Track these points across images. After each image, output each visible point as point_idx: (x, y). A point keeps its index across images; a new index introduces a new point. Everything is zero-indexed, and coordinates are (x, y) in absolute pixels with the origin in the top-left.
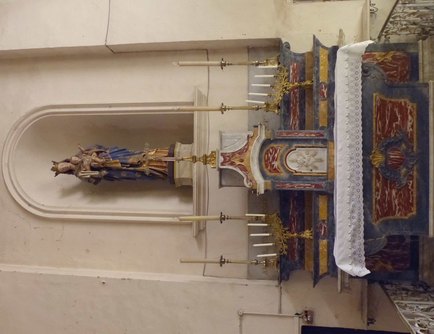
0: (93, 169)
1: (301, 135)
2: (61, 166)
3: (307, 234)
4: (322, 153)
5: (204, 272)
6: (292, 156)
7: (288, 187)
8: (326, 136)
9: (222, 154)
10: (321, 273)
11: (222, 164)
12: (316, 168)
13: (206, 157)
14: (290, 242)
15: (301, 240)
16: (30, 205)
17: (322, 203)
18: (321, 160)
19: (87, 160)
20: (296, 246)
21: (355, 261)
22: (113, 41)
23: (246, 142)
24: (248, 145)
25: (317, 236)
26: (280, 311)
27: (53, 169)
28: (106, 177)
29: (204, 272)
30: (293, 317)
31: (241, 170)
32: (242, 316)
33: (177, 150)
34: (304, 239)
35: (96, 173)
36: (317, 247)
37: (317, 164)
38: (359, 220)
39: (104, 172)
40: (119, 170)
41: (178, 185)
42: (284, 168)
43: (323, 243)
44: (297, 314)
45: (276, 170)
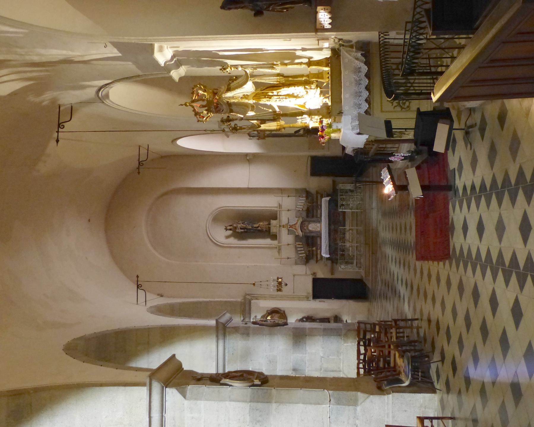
0: (241, 229)
1: (312, 219)
2: (229, 228)
3: (314, 249)
4: (318, 225)
5: (467, 120)
6: (310, 225)
7: (309, 235)
8: (320, 220)
9: (289, 225)
10: (318, 259)
11: (289, 228)
12: (317, 229)
13: (283, 225)
14: (309, 251)
15: (313, 251)
16: (217, 242)
17: (319, 239)
18: (318, 227)
19: (239, 226)
20: (311, 252)
21: (326, 254)
22: (250, 186)
23: (296, 222)
24: (297, 222)
25: (317, 249)
26: (306, 273)
27: (225, 229)
28: (245, 232)
29: (467, 120)
30: (310, 275)
31: (295, 230)
32: (294, 276)
33: (271, 223)
34: (313, 250)
35: (243, 230)
36: (317, 252)
37: (317, 228)
38: (327, 243)
39: (245, 230)
40: (250, 229)
41: (271, 234)
42: (308, 229)
43: (319, 251)
44: (311, 274)
45: (305, 230)
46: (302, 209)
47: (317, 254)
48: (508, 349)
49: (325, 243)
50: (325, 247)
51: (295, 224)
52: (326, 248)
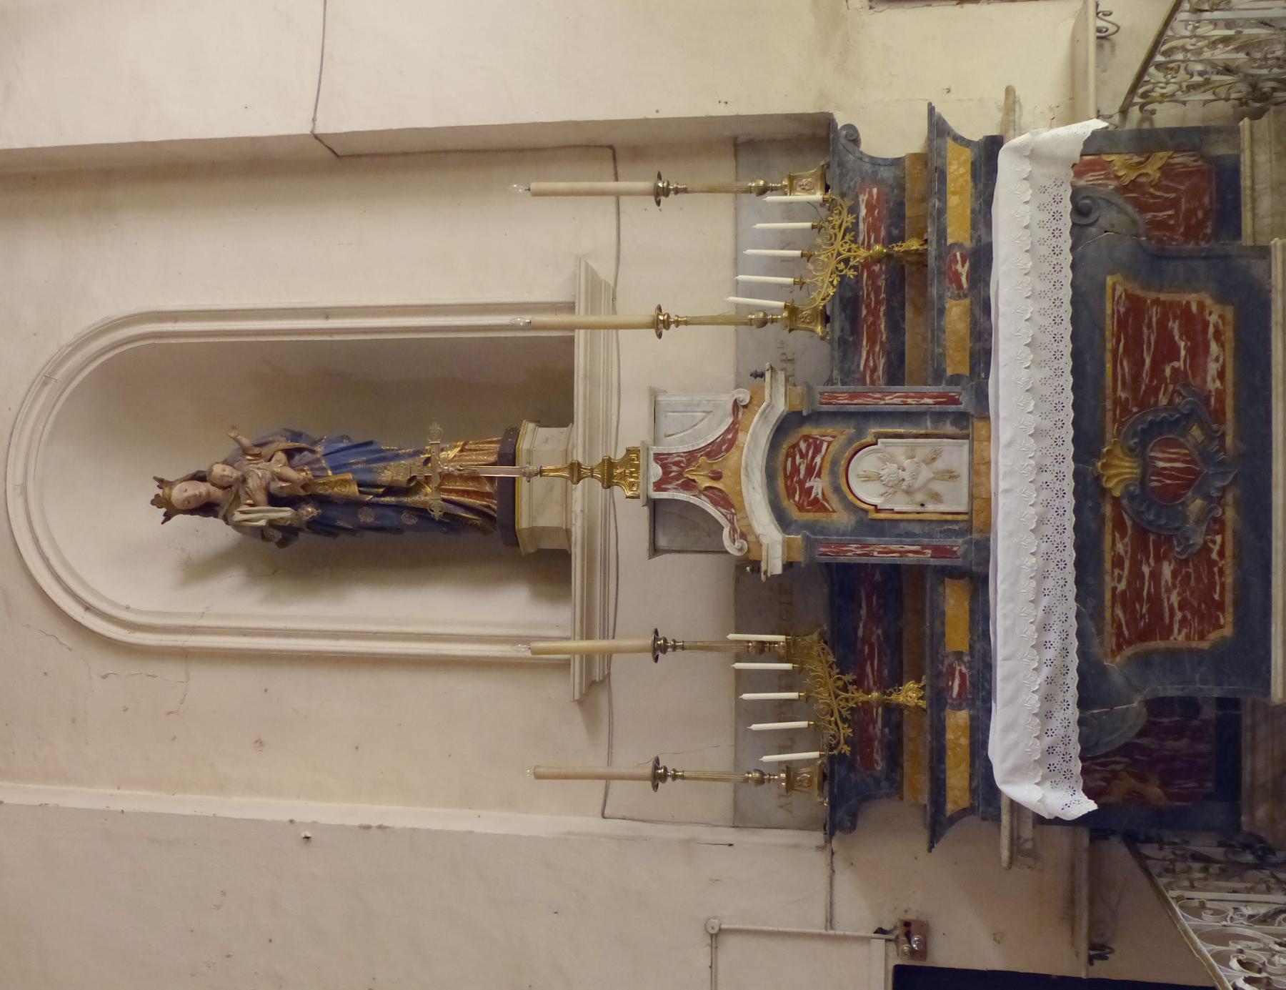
0: (275, 500)
1: (893, 399)
2: (180, 493)
3: (909, 694)
4: (955, 454)
5: (604, 806)
6: (865, 462)
7: (852, 553)
8: (966, 403)
9: (659, 458)
10: (950, 808)
11: (659, 486)
12: (936, 497)
13: (609, 464)
14: (858, 719)
15: (893, 713)
16: (88, 608)
17: (954, 602)
18: (951, 476)
19: (258, 474)
20: (878, 729)
21: (1051, 772)
22: (336, 122)
23: (730, 420)
24: (734, 428)
25: (938, 700)
26: (830, 921)
27: (157, 502)
28: (316, 526)
29: (604, 806)
30: (867, 940)
31: (715, 503)
32: (716, 936)
33: (524, 444)
34: (900, 709)
35: (285, 513)
36: (939, 731)
37: (939, 487)
38: (1065, 652)
39: (309, 511)
40: (352, 504)
41: (528, 547)
42: (843, 498)
43: (958, 719)
44: (880, 931)
45: (817, 505)
48: (1079, 720)
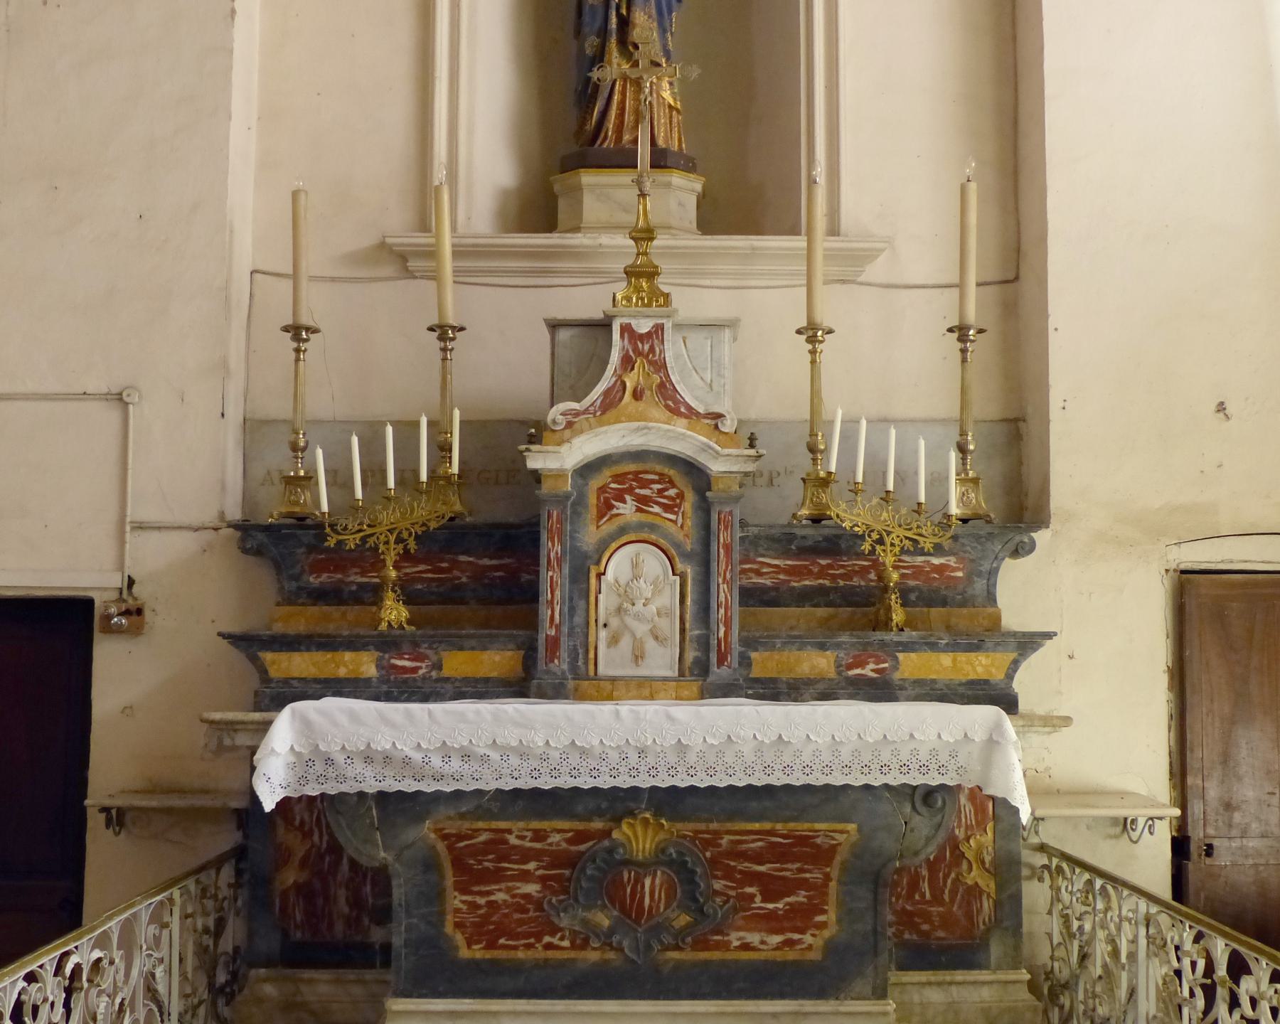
1: (724, 593)
3: (394, 612)
4: (661, 662)
5: (264, 273)
6: (653, 562)
7: (551, 548)
9: (659, 329)
10: (268, 656)
11: (626, 329)
12: (614, 641)
14: (368, 557)
15: (372, 595)
18: (638, 657)
21: (304, 762)
24: (691, 413)
25: (388, 643)
26: (140, 527)
30: (121, 567)
31: (607, 393)
32: (119, 399)
33: (677, 178)
34: (377, 601)
36: (354, 644)
37: (626, 643)
41: (559, 183)
42: (613, 537)
43: (366, 665)
44: (131, 582)
45: (606, 508)
46: (825, 482)
47: (327, 643)
49: (446, 752)
50: (383, 743)
51: (666, 391)
52: (368, 757)
